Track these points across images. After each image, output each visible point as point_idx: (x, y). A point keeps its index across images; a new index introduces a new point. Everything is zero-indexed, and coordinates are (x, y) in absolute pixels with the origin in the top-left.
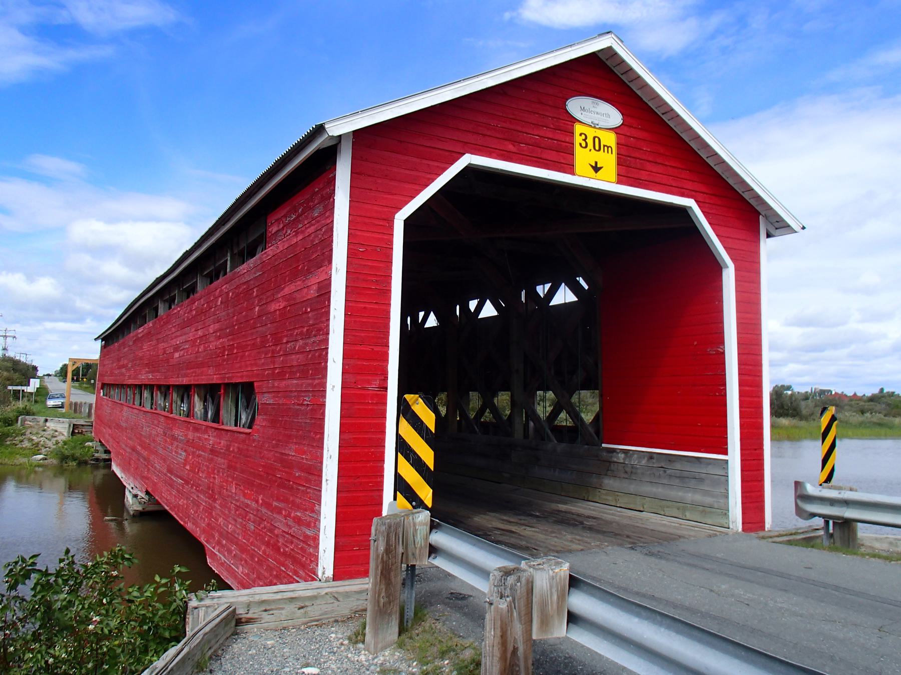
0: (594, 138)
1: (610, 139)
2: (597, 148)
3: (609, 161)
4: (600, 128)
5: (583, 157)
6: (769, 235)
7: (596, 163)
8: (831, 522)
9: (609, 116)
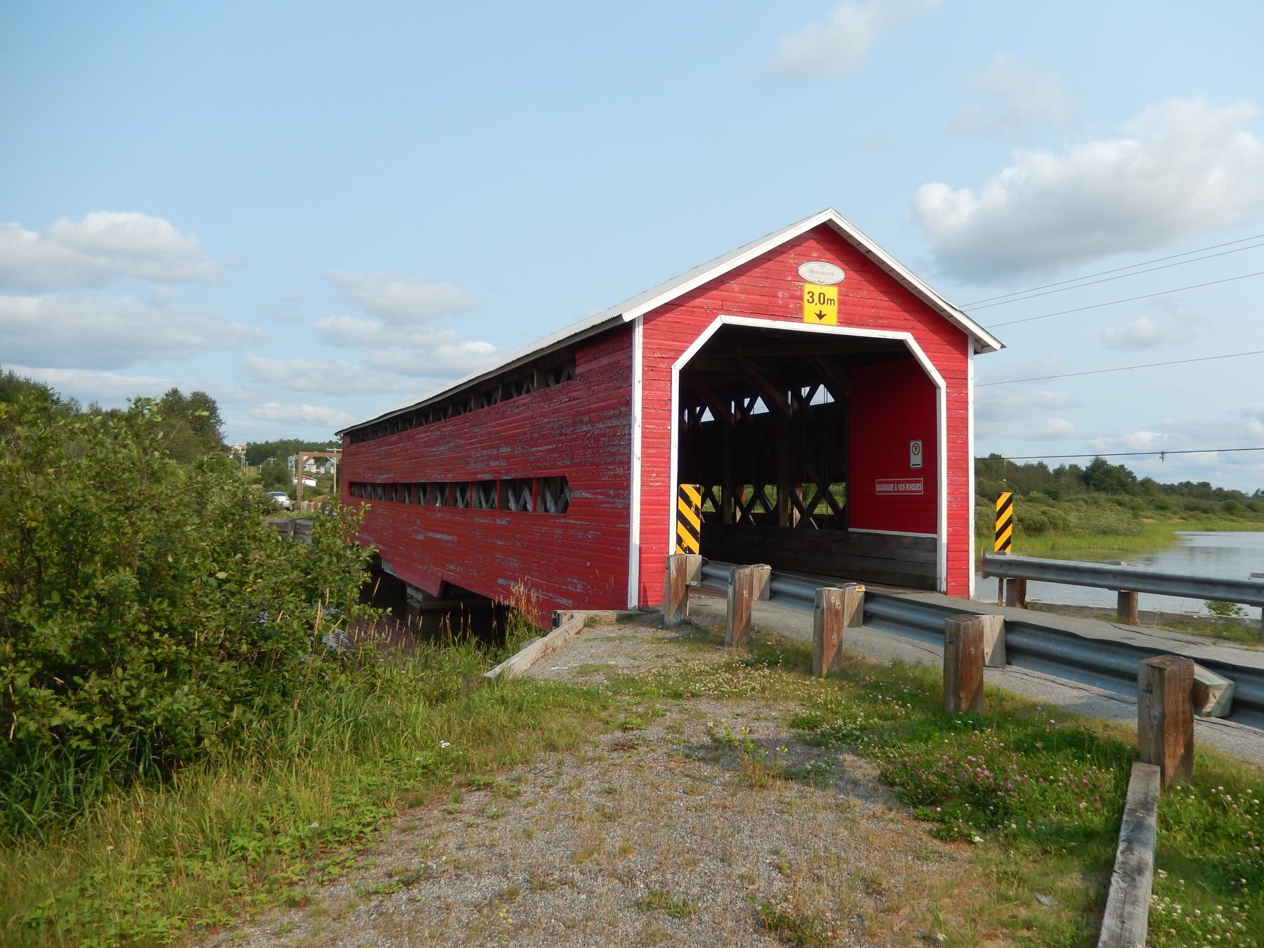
0: (820, 294)
1: (833, 293)
2: (822, 302)
3: (832, 311)
4: (826, 285)
5: (810, 310)
6: (976, 353)
7: (821, 312)
8: (1005, 581)
9: (833, 274)
